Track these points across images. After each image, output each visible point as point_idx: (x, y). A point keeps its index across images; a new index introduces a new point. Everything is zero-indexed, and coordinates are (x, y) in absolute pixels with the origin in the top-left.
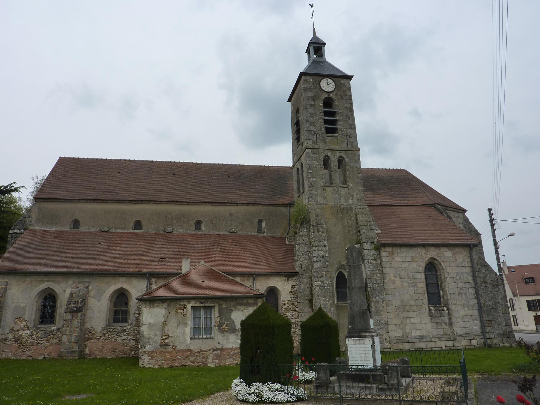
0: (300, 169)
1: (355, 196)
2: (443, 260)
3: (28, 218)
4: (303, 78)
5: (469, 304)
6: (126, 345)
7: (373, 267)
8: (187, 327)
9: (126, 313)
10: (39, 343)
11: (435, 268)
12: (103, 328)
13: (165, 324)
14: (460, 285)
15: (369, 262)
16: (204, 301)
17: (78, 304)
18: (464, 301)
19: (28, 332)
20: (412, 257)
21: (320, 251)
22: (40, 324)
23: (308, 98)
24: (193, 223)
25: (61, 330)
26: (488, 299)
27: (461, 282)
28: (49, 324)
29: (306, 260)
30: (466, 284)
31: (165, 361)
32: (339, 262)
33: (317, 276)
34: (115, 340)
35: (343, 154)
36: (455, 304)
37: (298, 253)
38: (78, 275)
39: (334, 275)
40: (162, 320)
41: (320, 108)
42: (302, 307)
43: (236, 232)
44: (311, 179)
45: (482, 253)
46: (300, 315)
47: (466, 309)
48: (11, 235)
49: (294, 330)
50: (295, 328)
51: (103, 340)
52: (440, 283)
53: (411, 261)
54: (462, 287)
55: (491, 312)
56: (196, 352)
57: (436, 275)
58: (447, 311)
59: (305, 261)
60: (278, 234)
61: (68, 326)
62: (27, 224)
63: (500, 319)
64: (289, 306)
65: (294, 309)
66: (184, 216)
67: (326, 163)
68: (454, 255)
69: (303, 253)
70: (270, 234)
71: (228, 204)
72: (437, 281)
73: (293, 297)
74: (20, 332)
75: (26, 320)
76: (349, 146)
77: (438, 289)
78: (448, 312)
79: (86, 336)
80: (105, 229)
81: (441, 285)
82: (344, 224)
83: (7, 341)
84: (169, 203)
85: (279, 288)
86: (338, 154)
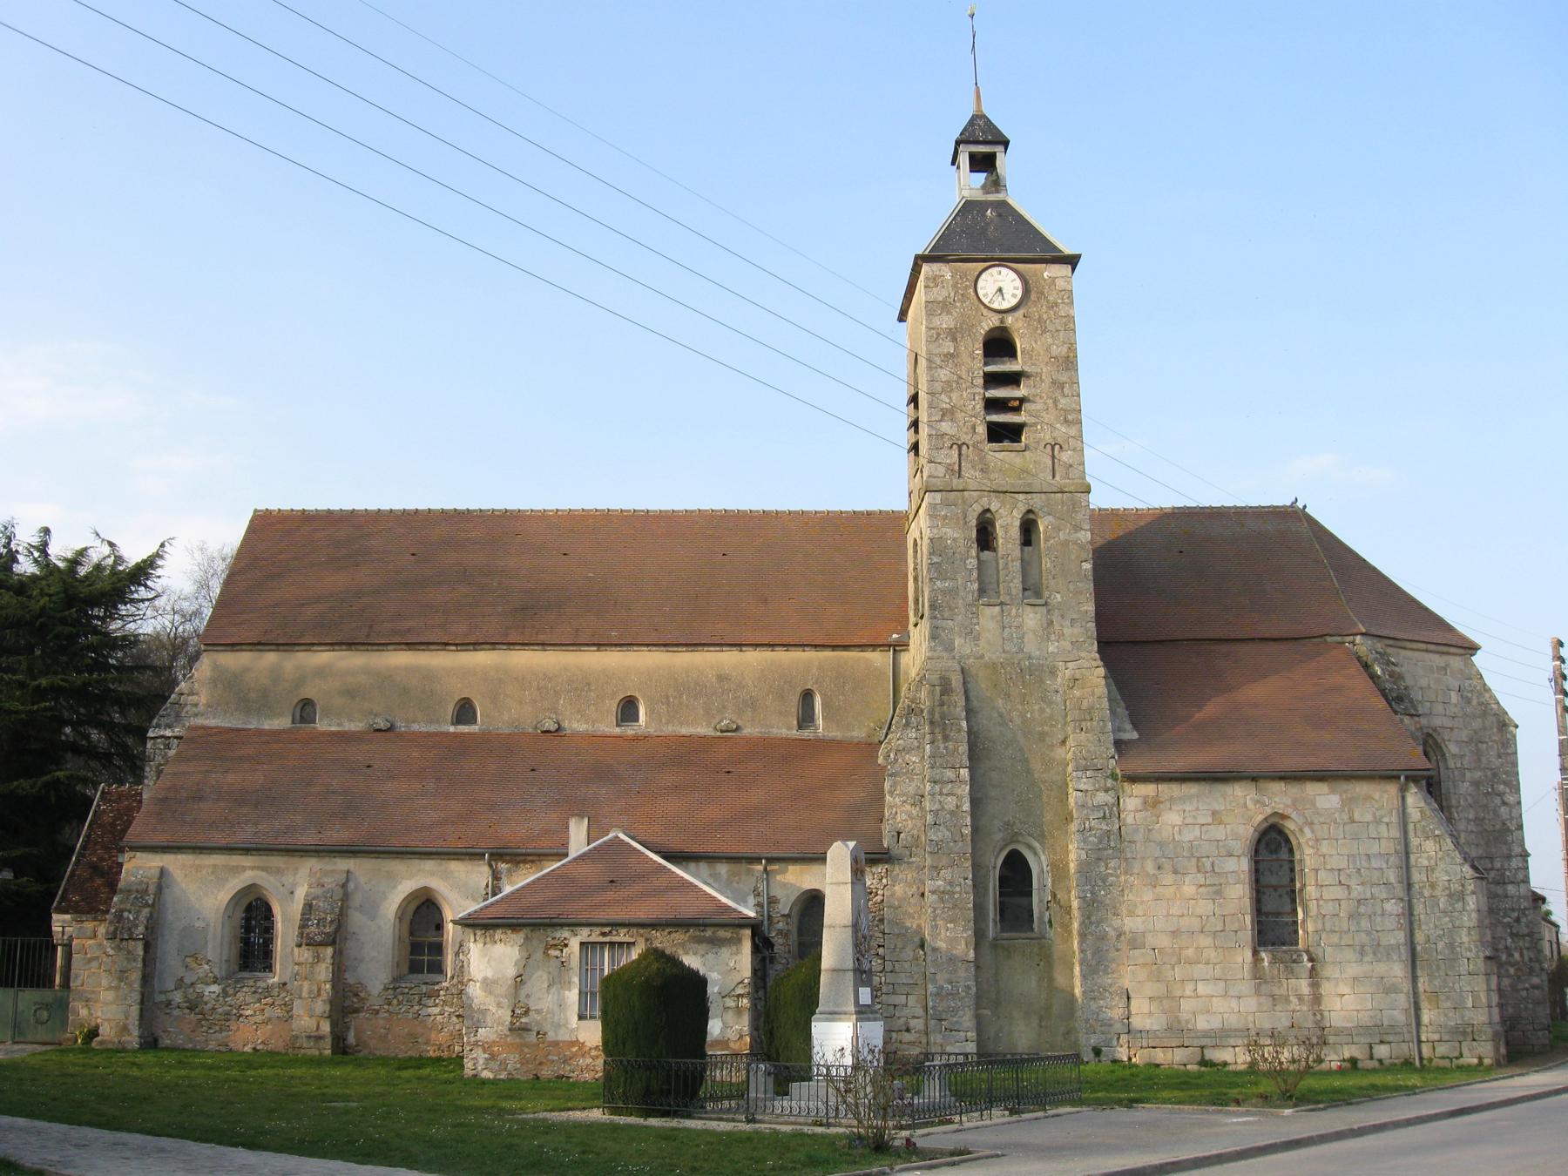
0: (919, 541)
2: (1309, 821)
3: (190, 698)
4: (926, 268)
5: (1379, 945)
6: (440, 1027)
7: (1096, 840)
8: (570, 991)
9: (438, 949)
10: (241, 1015)
11: (1288, 841)
12: (385, 985)
13: (519, 981)
14: (1357, 891)
16: (610, 932)
17: (325, 926)
18: (1364, 938)
19: (215, 988)
20: (1214, 813)
21: (947, 795)
22: (240, 971)
23: (938, 334)
24: (612, 705)
25: (288, 987)
26: (1435, 933)
27: (1362, 884)
28: (260, 971)
29: (912, 818)
30: (1375, 890)
31: (522, 1064)
32: (1008, 823)
34: (416, 1016)
35: (1037, 501)
36: (1338, 946)
37: (891, 799)
38: (321, 854)
39: (993, 860)
40: (511, 972)
41: (976, 365)
42: (896, 945)
44: (938, 583)
45: (1514, 783)
46: (889, 968)
47: (1366, 959)
48: (152, 741)
51: (386, 1014)
52: (1298, 885)
53: (1209, 825)
54: (1362, 897)
55: (1438, 968)
56: (590, 1049)
57: (1292, 862)
58: (1310, 965)
59: (910, 822)
60: (858, 734)
61: (306, 978)
62: (187, 712)
63: (1460, 988)
66: (589, 684)
67: (985, 536)
68: (1348, 803)
69: (905, 798)
70: (836, 734)
72: (1293, 880)
74: (200, 987)
75: (210, 961)
76: (1057, 478)
77: (1294, 901)
78: (1312, 966)
79: (348, 1003)
80: (382, 725)
81: (1301, 890)
82: (1029, 716)
83: (171, 1009)
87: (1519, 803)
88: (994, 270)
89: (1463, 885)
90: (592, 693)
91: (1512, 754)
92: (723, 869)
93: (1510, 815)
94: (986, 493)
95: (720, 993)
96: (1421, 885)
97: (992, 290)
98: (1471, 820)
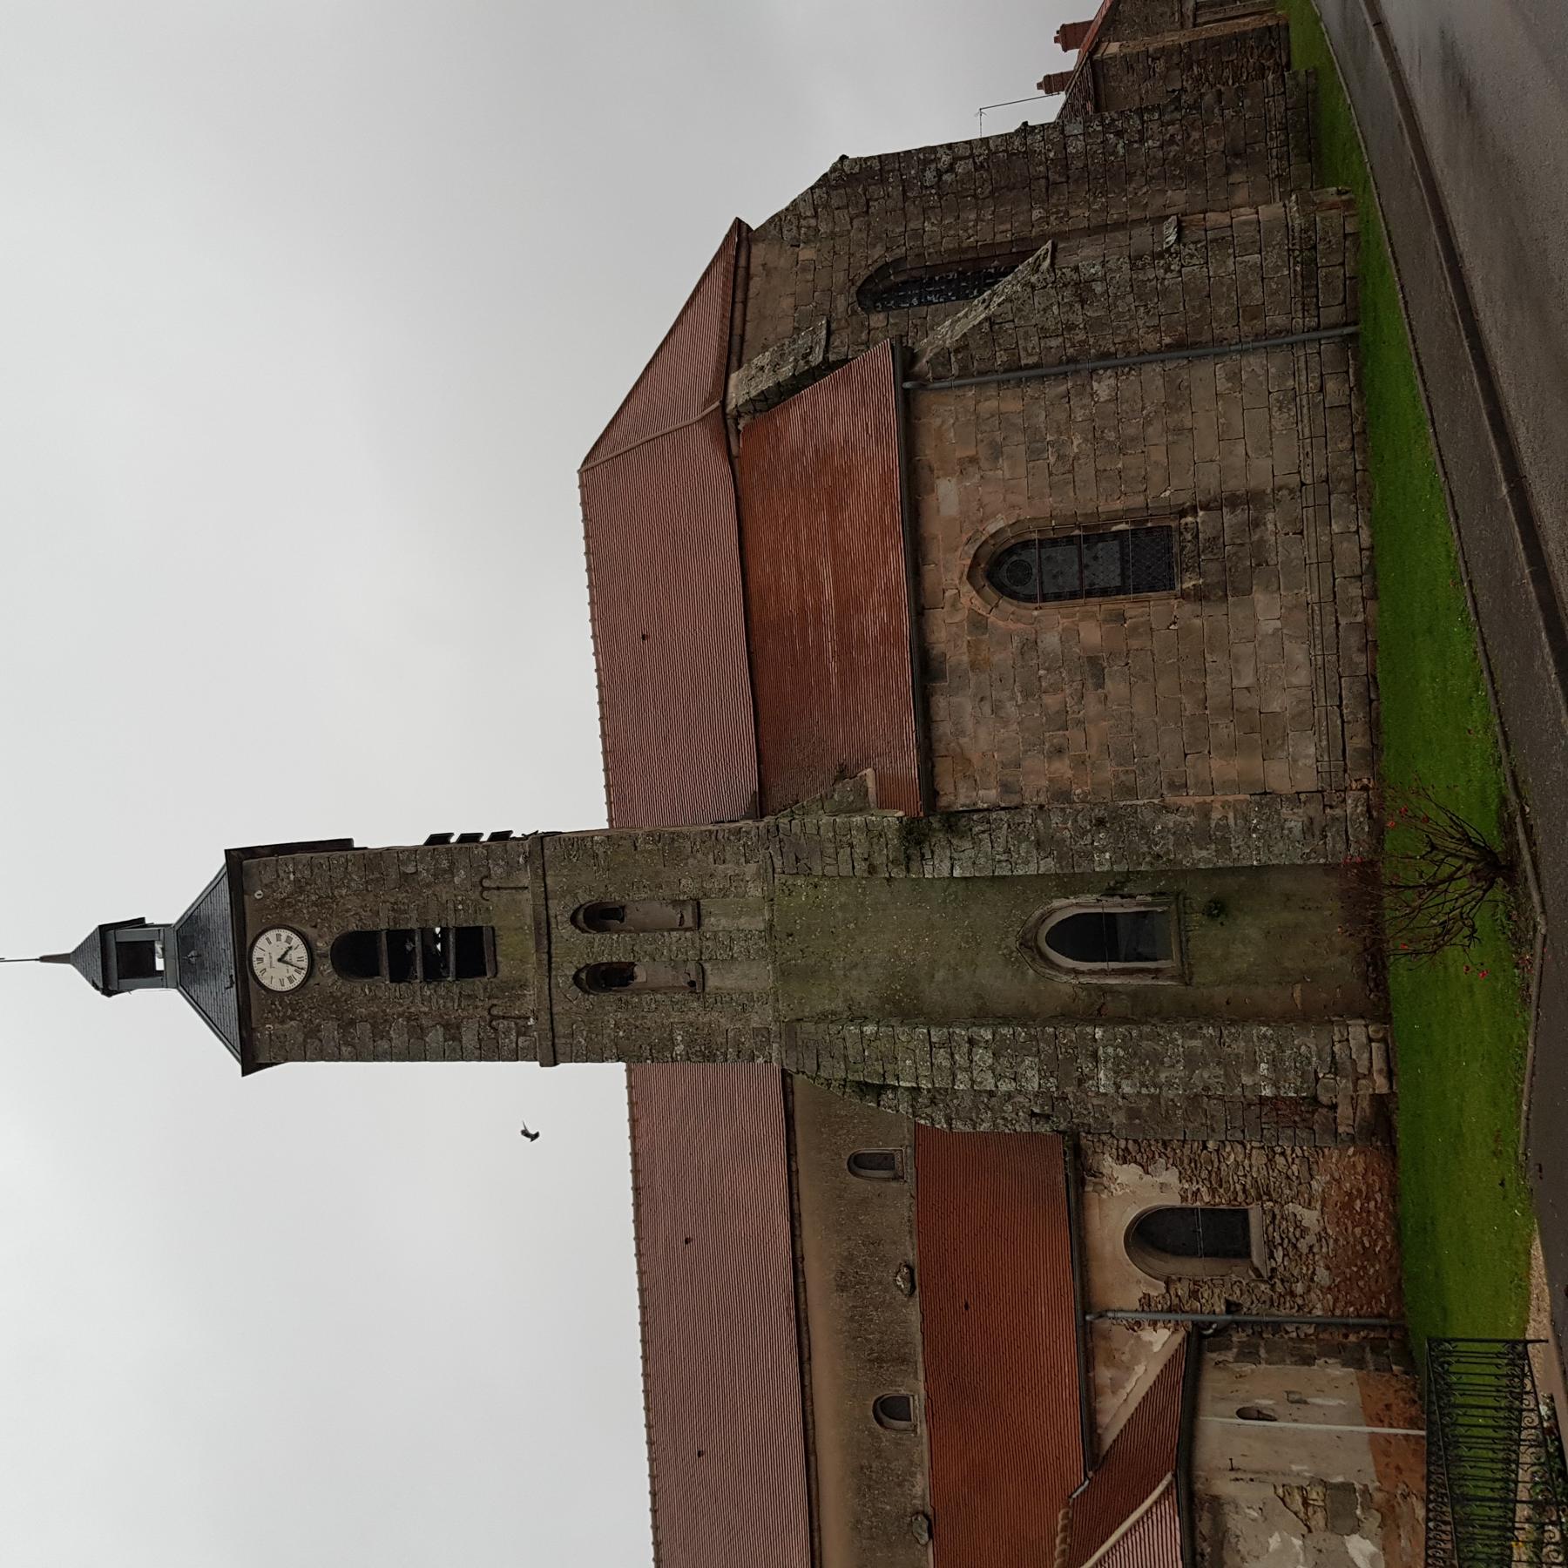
1: (730, 869)
15: (1003, 858)
33: (1075, 1083)
35: (560, 910)
43: (907, 1266)
49: (1297, 1161)
50: (1290, 1160)
59: (1016, 1100)
64: (1203, 1176)
65: (1214, 1157)
71: (802, 1296)
73: (1162, 1161)
84: (816, 1524)
85: (1132, 1213)
86: (564, 931)
87: (950, 146)
88: (257, 967)
89: (1065, 285)
90: (874, 1465)
91: (880, 162)
92: (1104, 1374)
93: (968, 158)
94: (553, 981)
95: (1303, 1536)
96: (1068, 345)
97: (283, 971)
98: (978, 215)
